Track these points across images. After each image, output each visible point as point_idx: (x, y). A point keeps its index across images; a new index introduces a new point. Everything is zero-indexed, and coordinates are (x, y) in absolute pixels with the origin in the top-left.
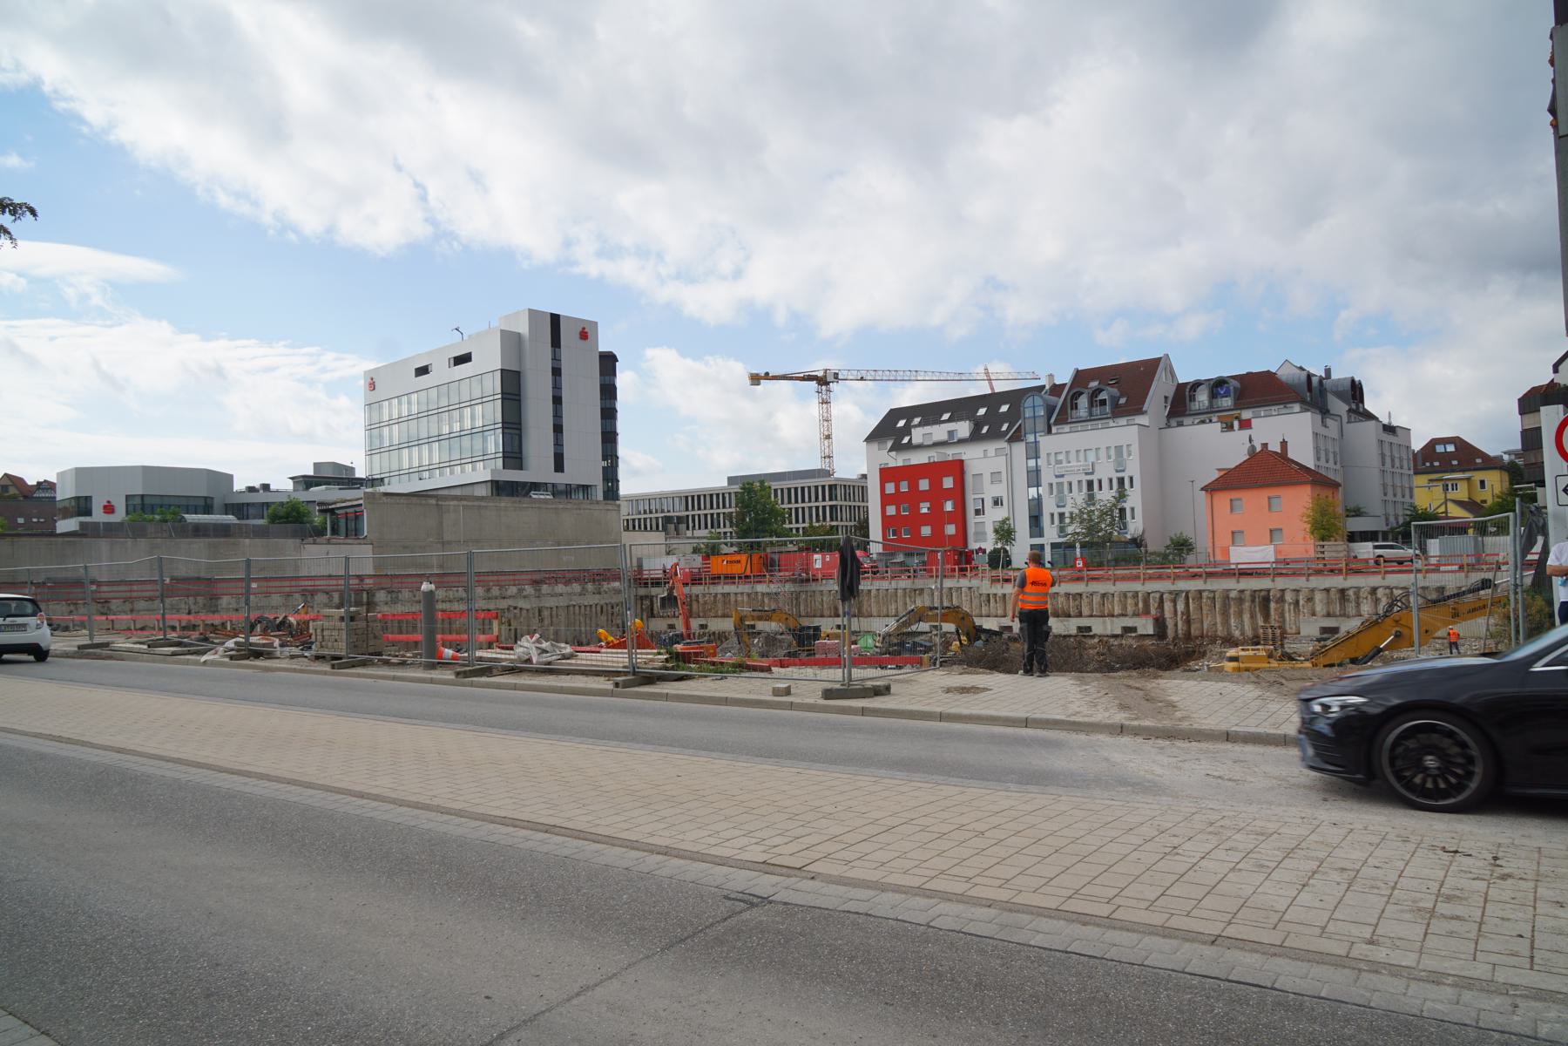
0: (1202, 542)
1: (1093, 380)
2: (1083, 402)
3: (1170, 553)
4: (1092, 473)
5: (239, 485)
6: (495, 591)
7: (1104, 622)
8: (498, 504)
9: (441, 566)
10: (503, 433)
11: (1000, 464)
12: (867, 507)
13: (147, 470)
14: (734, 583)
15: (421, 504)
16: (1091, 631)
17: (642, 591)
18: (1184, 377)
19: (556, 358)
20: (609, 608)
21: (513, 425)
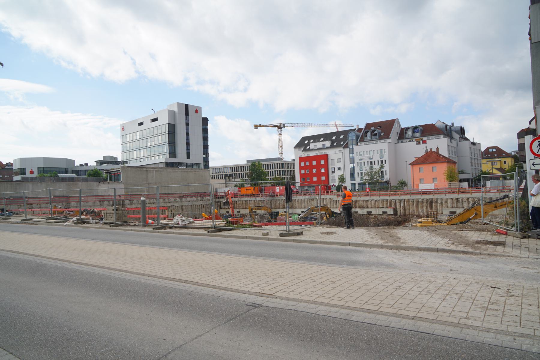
0: (409, 182)
1: (372, 127)
2: (369, 134)
4: (372, 159)
6: (167, 200)
7: (376, 210)
10: (169, 145)
11: (340, 156)
12: (295, 171)
13: (45, 159)
14: (249, 197)
19: (187, 120)
21: (172, 143)
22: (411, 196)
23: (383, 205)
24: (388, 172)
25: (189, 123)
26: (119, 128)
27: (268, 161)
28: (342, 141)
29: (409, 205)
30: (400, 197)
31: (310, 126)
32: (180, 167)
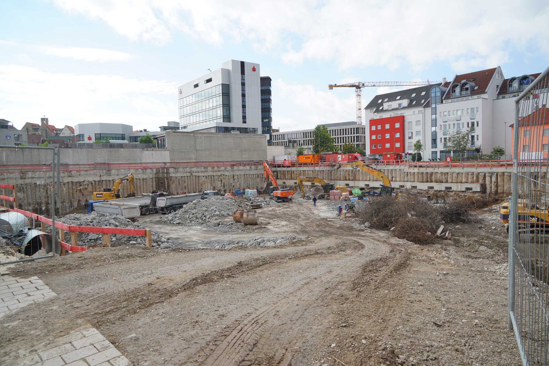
0: (509, 150)
1: (464, 79)
2: (458, 90)
3: (493, 155)
4: (460, 120)
5: (134, 129)
6: (216, 169)
7: (457, 185)
8: (218, 136)
9: (196, 159)
10: (223, 109)
11: (420, 117)
12: (365, 136)
13: (102, 125)
14: (307, 166)
15: (187, 136)
16: (451, 189)
17: (274, 169)
18: (507, 76)
19: (243, 79)
20: (261, 176)
21: (227, 105)
22: (506, 169)
23: (468, 179)
24: (480, 138)
25: (245, 83)
26: (176, 91)
27: (353, 125)
28: (423, 99)
29: (504, 180)
30: (491, 169)
31: (395, 85)
32: (232, 132)
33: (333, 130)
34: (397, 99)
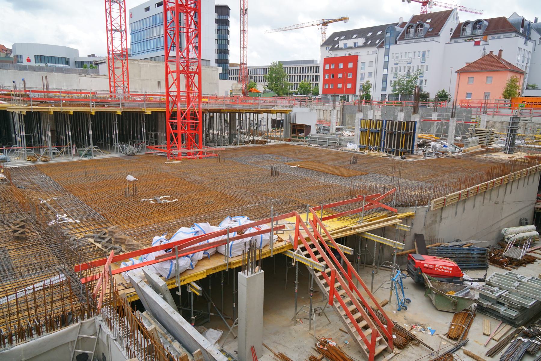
4: (410, 63)
11: (373, 58)
33: (293, 68)
34: (353, 37)
